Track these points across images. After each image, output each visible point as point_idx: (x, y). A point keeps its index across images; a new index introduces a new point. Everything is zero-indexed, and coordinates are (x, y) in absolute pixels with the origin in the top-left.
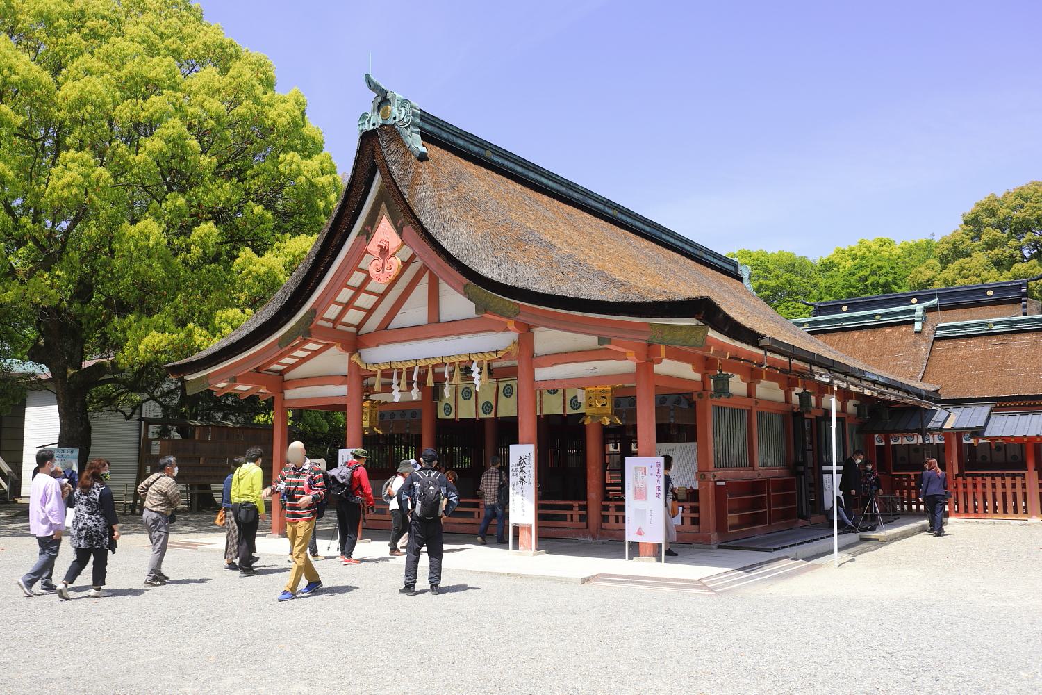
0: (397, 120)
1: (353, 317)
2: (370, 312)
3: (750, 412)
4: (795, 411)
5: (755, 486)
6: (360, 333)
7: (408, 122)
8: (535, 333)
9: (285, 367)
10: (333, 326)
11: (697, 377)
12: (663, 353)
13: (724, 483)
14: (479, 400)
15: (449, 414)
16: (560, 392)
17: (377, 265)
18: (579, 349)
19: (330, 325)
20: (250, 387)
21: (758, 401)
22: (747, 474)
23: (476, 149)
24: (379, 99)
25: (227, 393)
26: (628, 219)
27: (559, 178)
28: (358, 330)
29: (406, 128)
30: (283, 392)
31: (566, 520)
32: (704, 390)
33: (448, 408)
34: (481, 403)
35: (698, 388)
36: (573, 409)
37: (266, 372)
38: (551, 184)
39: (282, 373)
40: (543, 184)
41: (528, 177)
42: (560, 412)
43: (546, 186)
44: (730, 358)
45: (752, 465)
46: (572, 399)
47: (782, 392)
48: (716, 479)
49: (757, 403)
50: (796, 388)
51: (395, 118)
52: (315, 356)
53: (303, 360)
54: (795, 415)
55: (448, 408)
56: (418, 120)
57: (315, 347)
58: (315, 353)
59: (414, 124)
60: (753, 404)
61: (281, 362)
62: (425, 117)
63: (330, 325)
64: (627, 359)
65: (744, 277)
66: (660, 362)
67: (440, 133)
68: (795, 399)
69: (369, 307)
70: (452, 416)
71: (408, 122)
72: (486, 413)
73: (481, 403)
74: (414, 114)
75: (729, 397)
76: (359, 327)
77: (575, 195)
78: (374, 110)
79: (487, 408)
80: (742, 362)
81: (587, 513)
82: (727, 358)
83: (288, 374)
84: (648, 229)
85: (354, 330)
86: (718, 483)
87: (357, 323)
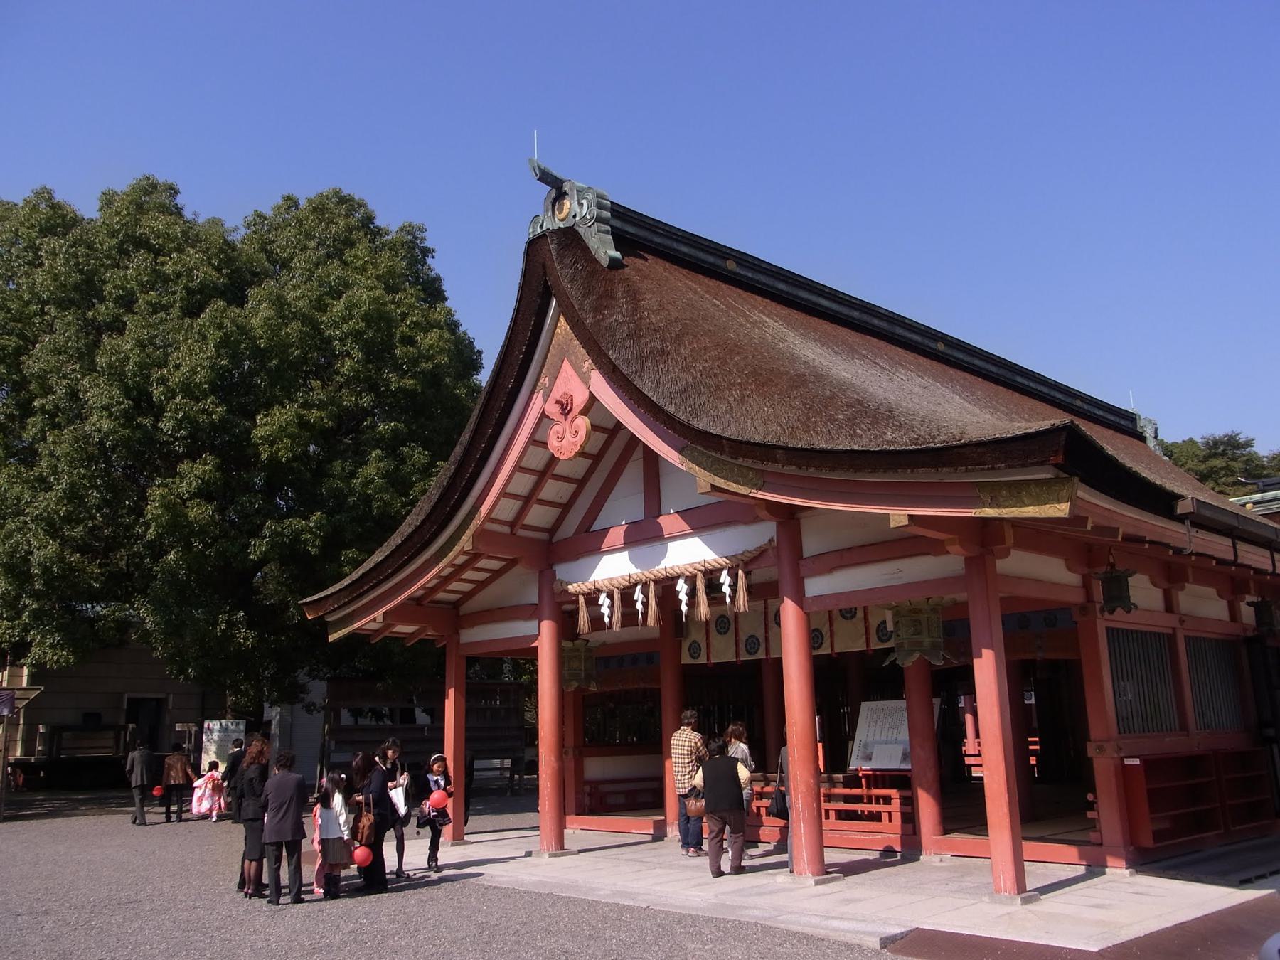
0: (577, 218)
1: (539, 516)
2: (565, 508)
3: (1172, 638)
4: (1250, 634)
5: (1190, 763)
6: (555, 539)
7: (592, 219)
8: (802, 521)
9: (461, 596)
10: (512, 531)
11: (1074, 579)
12: (1010, 540)
13: (1137, 761)
14: (741, 633)
15: (756, 652)
16: (860, 614)
17: (558, 432)
18: (873, 542)
19: (506, 530)
20: (417, 628)
21: (1184, 618)
22: (1172, 744)
23: (711, 259)
24: (553, 194)
25: (421, 639)
26: (961, 356)
27: (847, 298)
28: (551, 537)
29: (590, 226)
30: (457, 633)
31: (880, 820)
32: (1088, 601)
33: (694, 650)
34: (743, 638)
35: (1078, 597)
36: (750, 653)
37: (430, 605)
38: (834, 306)
39: (456, 605)
40: (802, 299)
41: (797, 296)
42: (860, 646)
43: (827, 308)
44: (1123, 538)
45: (1184, 727)
46: (879, 626)
47: (1224, 603)
48: (1122, 755)
49: (1182, 622)
50: (1247, 596)
51: (575, 217)
52: (495, 580)
53: (481, 585)
54: (1248, 641)
55: (694, 650)
56: (607, 214)
57: (496, 565)
58: (496, 574)
59: (599, 220)
60: (1176, 624)
61: (448, 588)
62: (619, 212)
63: (506, 530)
64: (948, 553)
65: (1148, 435)
66: (1006, 554)
67: (624, 225)
68: (1247, 614)
69: (564, 500)
70: (702, 660)
71: (592, 219)
72: (694, 658)
73: (743, 638)
74: (600, 207)
75: (1128, 612)
76: (552, 530)
77: (876, 321)
78: (547, 211)
79: (753, 645)
80: (1147, 546)
81: (913, 808)
82: (1120, 539)
83: (464, 606)
84: (993, 369)
85: (544, 536)
86: (1128, 761)
87: (548, 526)
